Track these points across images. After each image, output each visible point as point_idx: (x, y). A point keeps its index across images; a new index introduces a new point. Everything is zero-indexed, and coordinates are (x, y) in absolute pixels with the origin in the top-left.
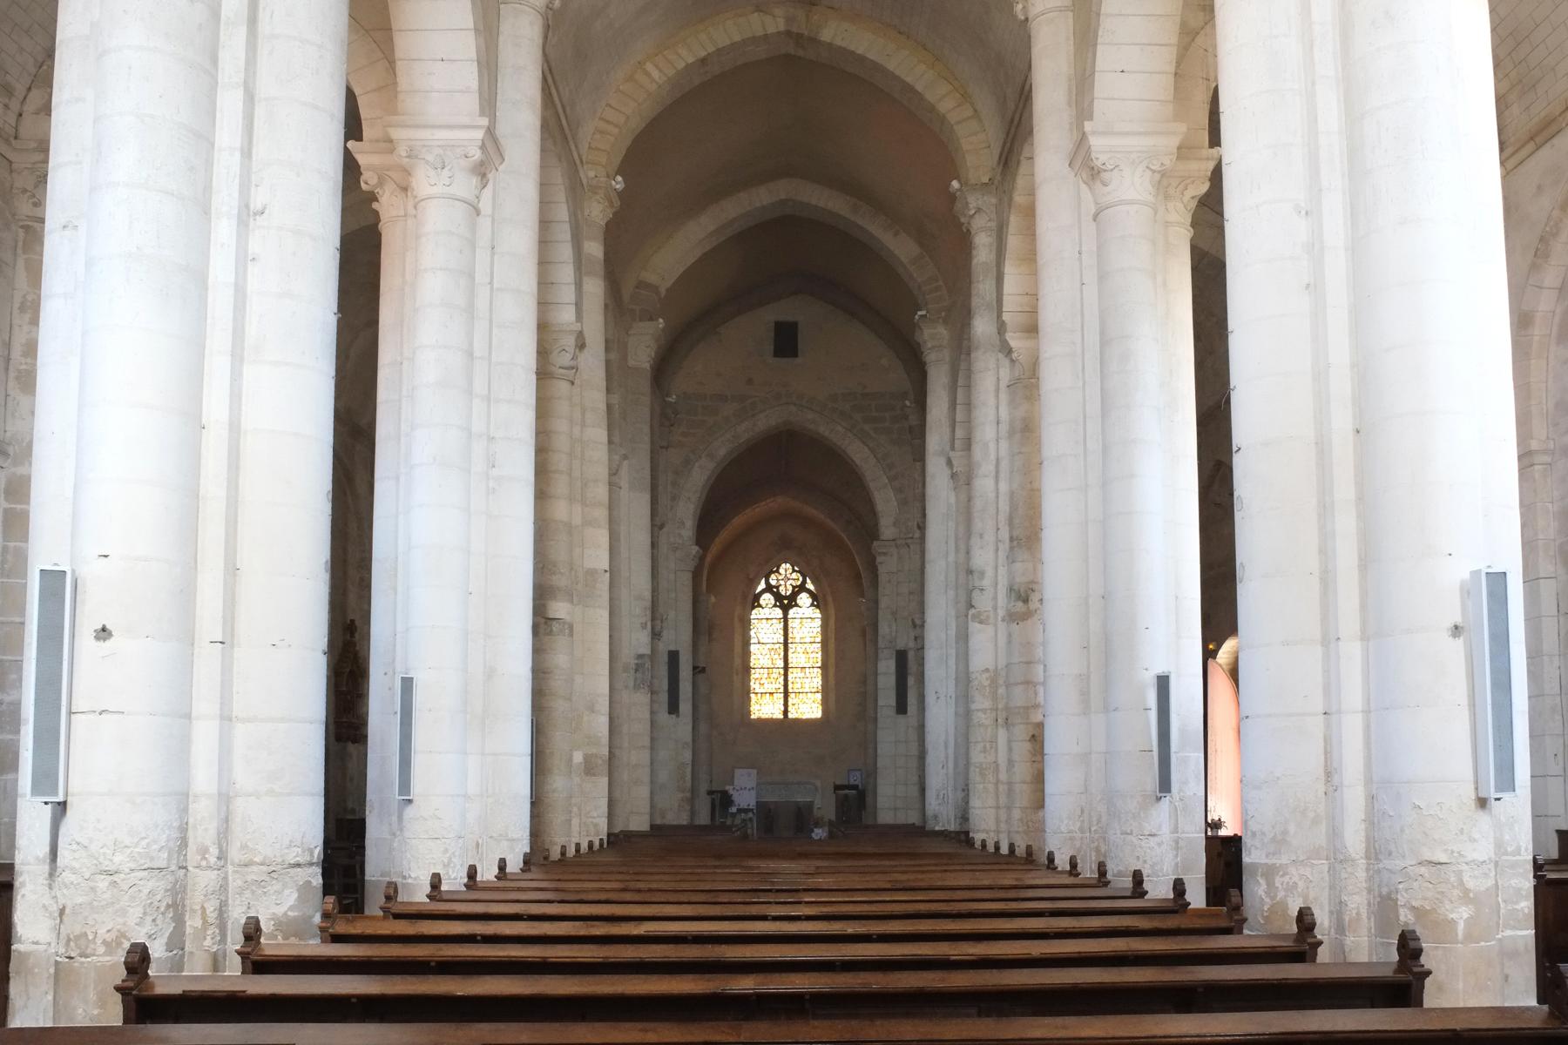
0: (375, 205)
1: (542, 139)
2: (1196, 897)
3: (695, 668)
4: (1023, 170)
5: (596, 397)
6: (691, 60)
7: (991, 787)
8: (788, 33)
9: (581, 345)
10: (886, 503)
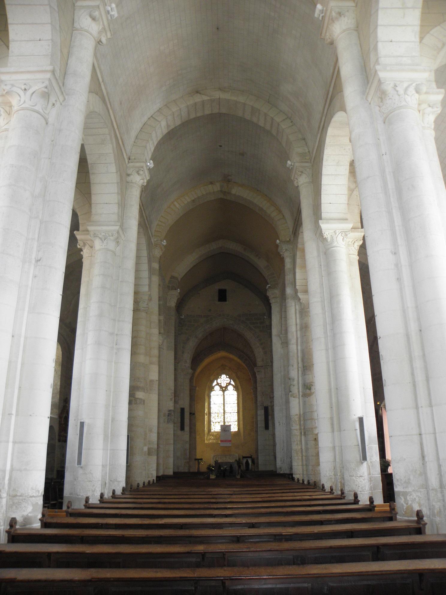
0: (82, 253)
1: (138, 228)
2: (379, 500)
3: (190, 414)
4: (300, 236)
5: (155, 318)
6: (189, 200)
7: (300, 457)
8: (221, 191)
9: (150, 300)
10: (259, 353)
